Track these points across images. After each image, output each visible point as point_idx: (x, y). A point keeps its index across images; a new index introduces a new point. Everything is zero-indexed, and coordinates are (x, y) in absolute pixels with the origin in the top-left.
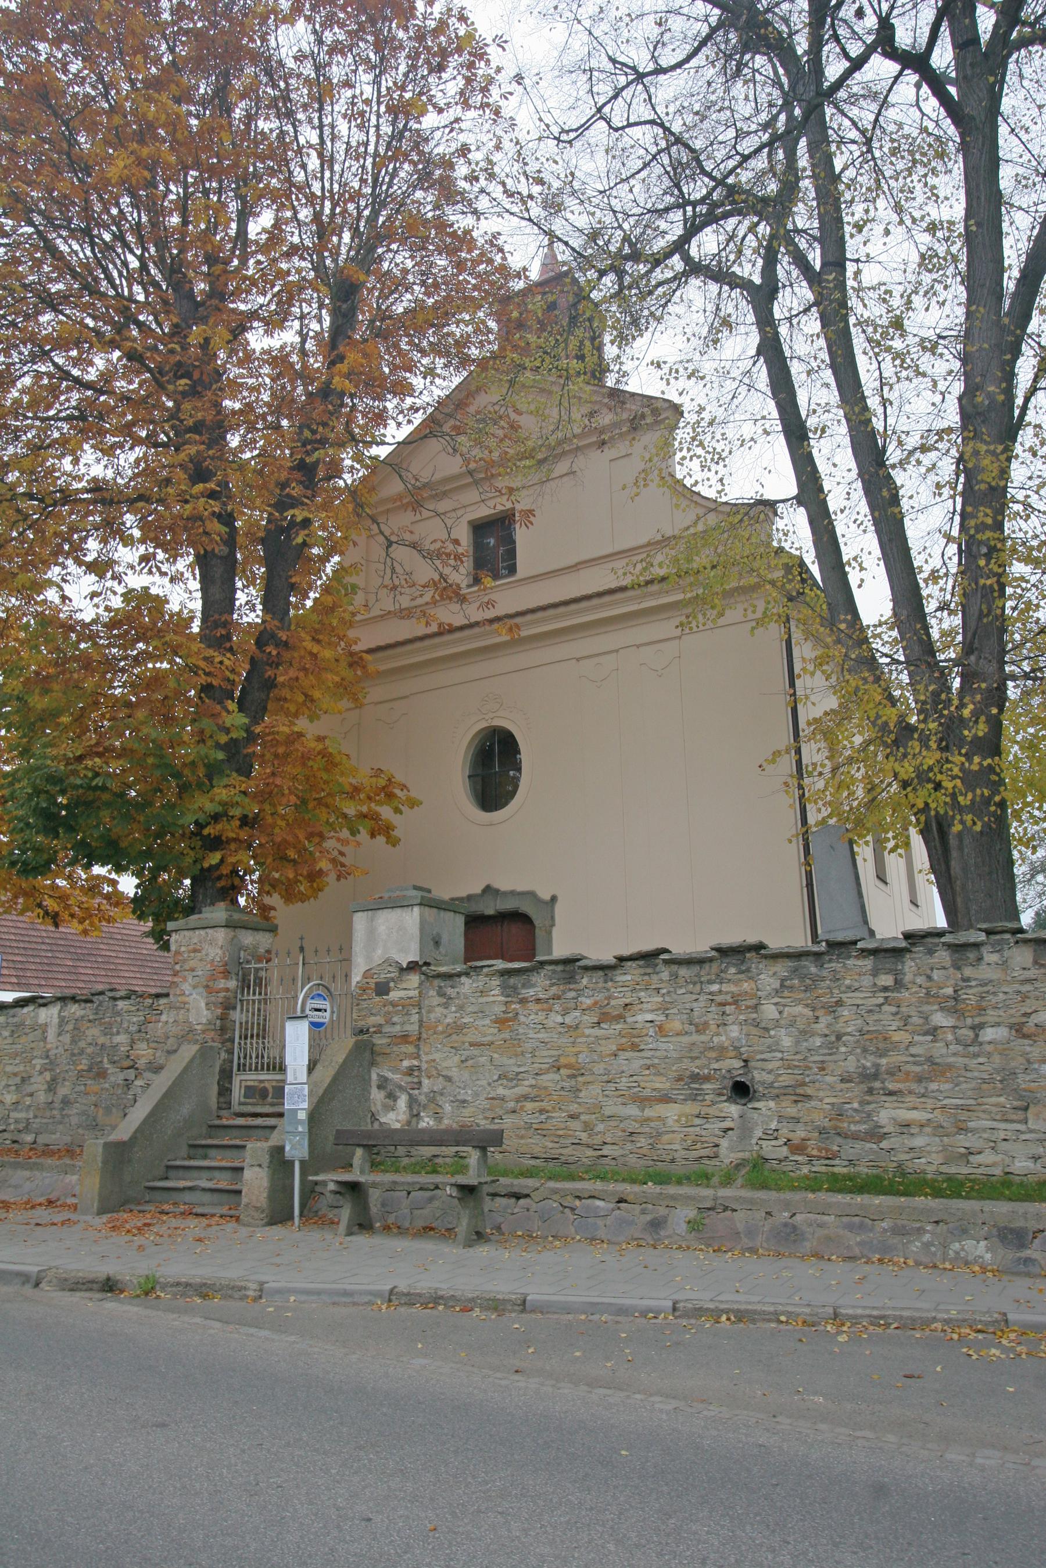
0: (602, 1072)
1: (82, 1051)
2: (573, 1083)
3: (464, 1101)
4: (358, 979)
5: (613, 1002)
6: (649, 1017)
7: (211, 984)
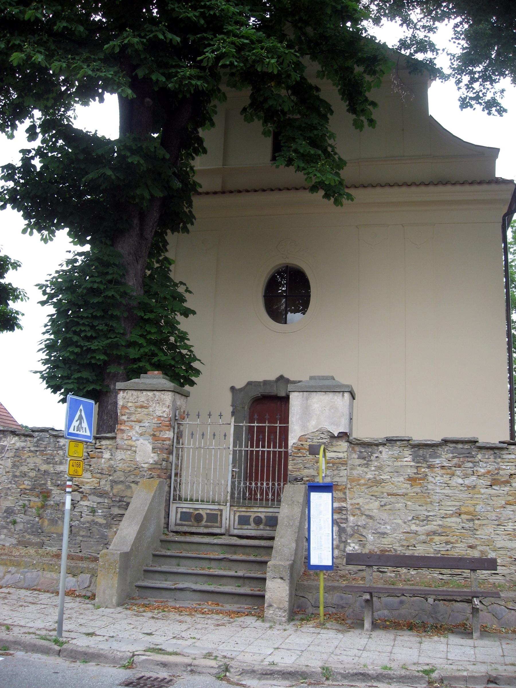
0: (494, 518)
1: (24, 475)
2: (471, 524)
3: (384, 533)
4: (295, 441)
5: (501, 472)
7: (157, 433)
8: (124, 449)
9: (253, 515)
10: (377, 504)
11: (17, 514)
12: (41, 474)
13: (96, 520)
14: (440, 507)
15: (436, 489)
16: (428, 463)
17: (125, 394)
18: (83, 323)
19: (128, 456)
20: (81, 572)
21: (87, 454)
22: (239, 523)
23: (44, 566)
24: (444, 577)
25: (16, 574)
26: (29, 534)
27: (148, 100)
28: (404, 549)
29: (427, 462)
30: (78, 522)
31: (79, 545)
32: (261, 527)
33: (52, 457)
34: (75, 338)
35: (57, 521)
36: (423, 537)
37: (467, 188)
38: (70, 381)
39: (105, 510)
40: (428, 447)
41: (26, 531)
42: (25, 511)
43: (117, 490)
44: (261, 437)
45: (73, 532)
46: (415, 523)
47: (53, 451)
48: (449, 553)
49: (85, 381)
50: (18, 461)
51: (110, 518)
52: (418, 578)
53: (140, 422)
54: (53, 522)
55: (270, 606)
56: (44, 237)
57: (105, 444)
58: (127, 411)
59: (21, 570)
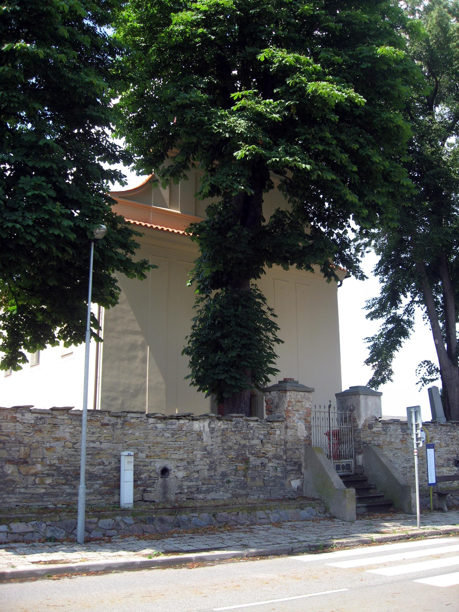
6: (437, 441)
10: (392, 454)
26: (238, 489)
53: (298, 411)
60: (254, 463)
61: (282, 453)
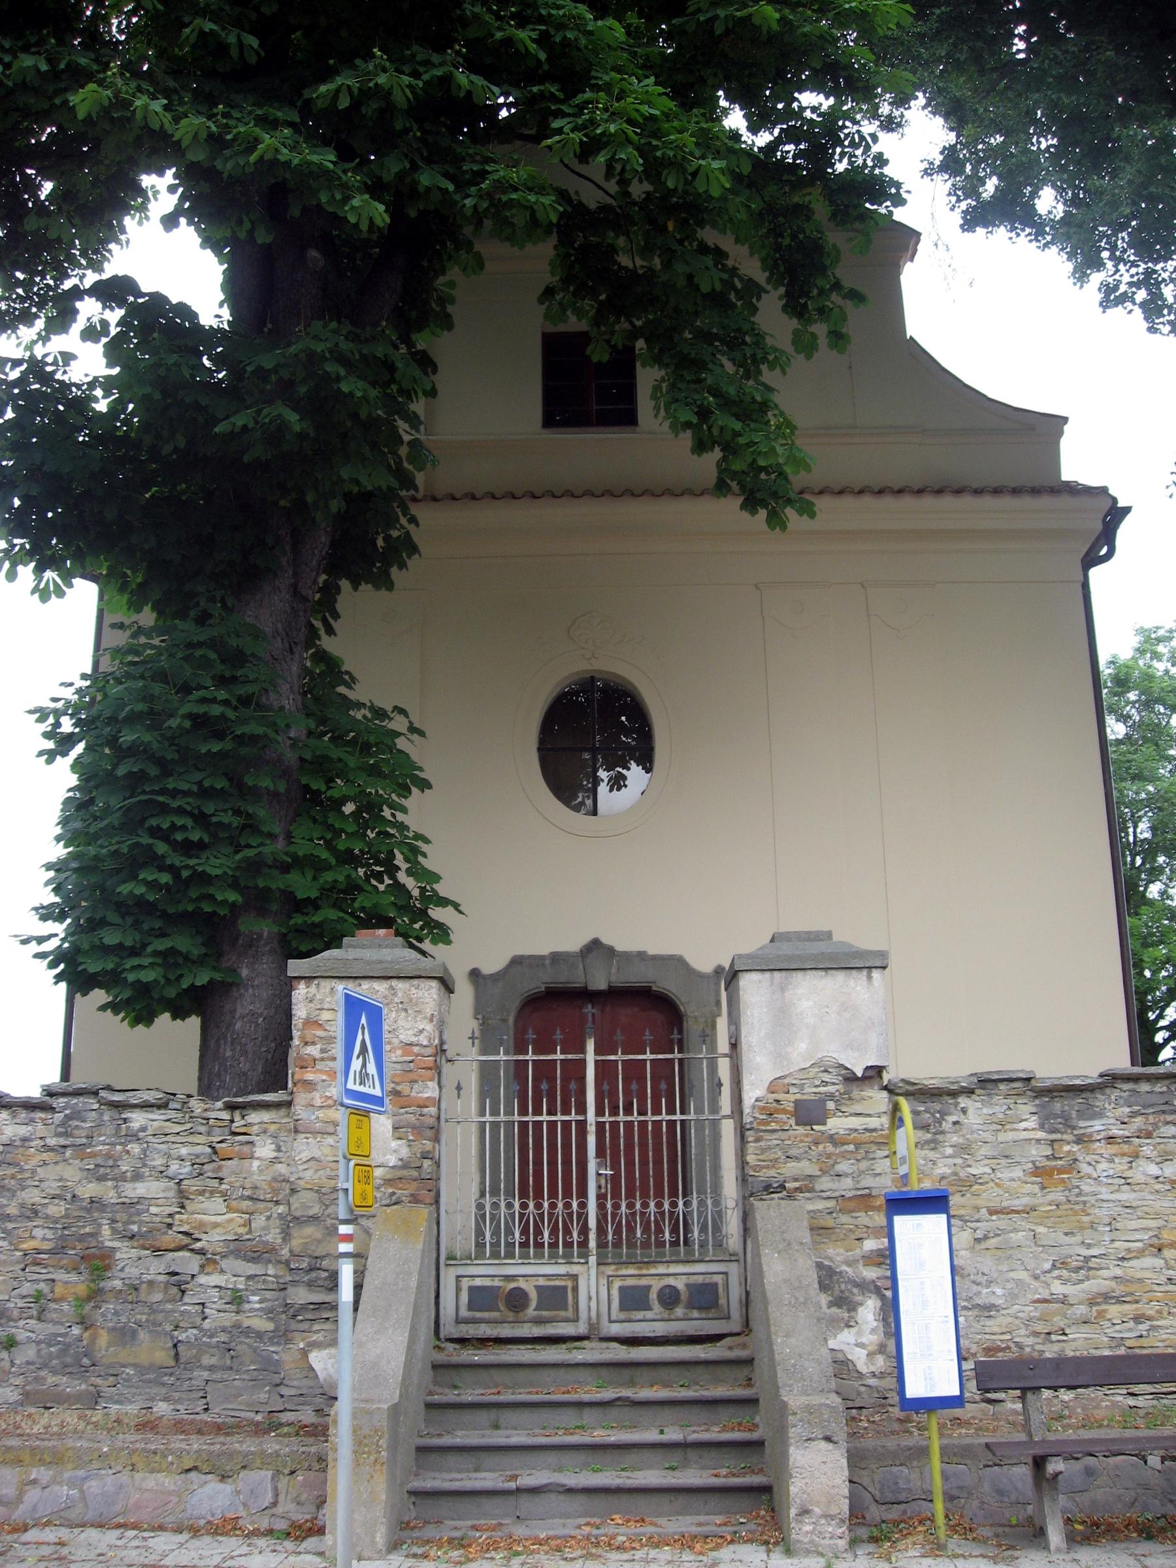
1: (32, 1212)
4: (759, 1092)
7: (404, 1088)
8: (315, 1133)
9: (656, 1285)
11: (15, 1321)
12: (82, 1208)
13: (247, 1323)
14: (1115, 1235)
15: (1100, 1193)
16: (1076, 1132)
17: (313, 989)
18: (179, 807)
19: (327, 1150)
20: (244, 1467)
21: (209, 1150)
22: (622, 1308)
23: (135, 1459)
24: (1140, 1402)
25: (57, 1488)
26: (54, 1372)
27: (313, 253)
28: (1039, 1340)
29: (1074, 1128)
30: (195, 1331)
31: (201, 1394)
32: (679, 1311)
33: (111, 1163)
34: (161, 848)
35: (134, 1333)
36: (1082, 1310)
37: (1007, 501)
38: (145, 961)
39: (268, 1295)
40: (1071, 1094)
41: (44, 1366)
42: (42, 1311)
43: (301, 1241)
44: (544, 1086)
45: (183, 1360)
46: (1059, 1278)
47: (113, 1144)
48: (1144, 1342)
49: (180, 960)
50: (13, 1177)
51: (283, 1316)
52: (1079, 1410)
54: (124, 1334)
55: (805, 1512)
56: (42, 585)
57: (256, 1121)
58: (320, 1033)
59: (66, 1475)
60: (132, 1271)
61: (273, 1236)
